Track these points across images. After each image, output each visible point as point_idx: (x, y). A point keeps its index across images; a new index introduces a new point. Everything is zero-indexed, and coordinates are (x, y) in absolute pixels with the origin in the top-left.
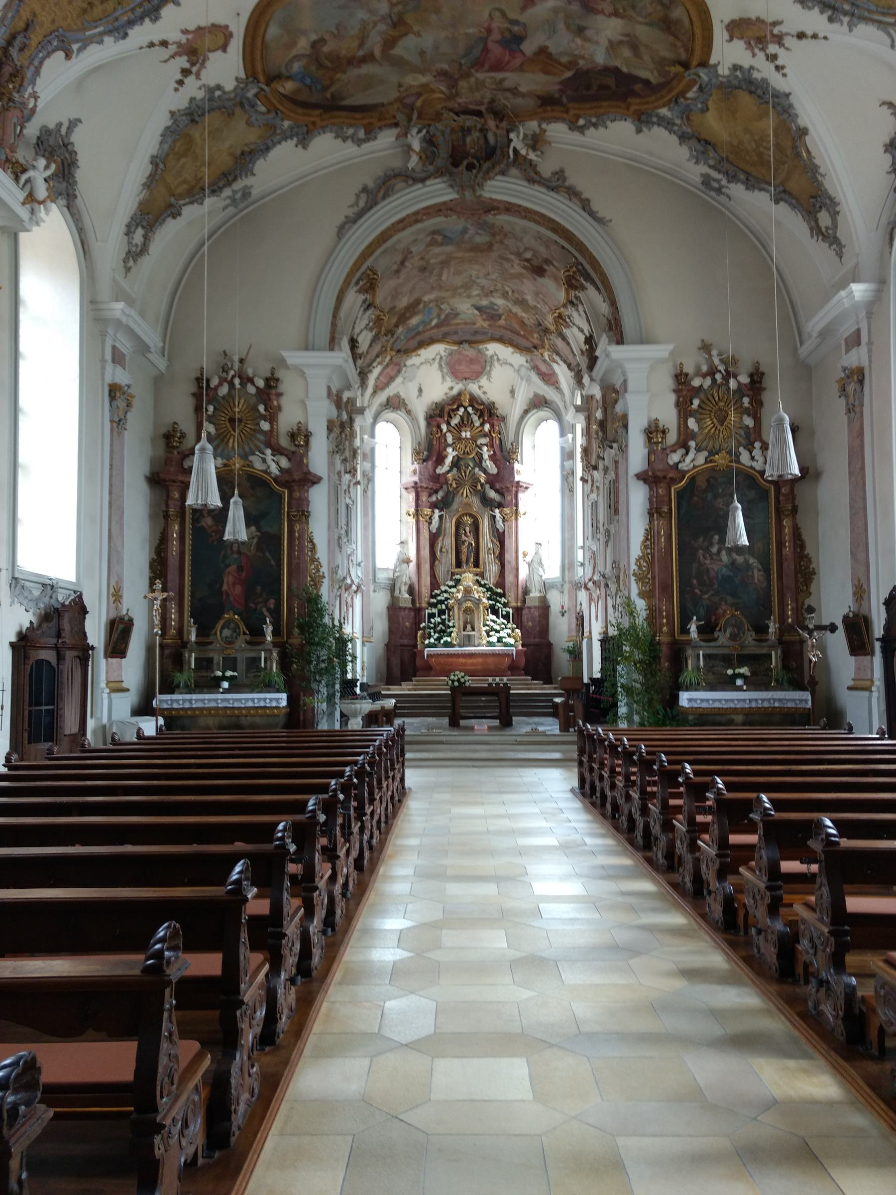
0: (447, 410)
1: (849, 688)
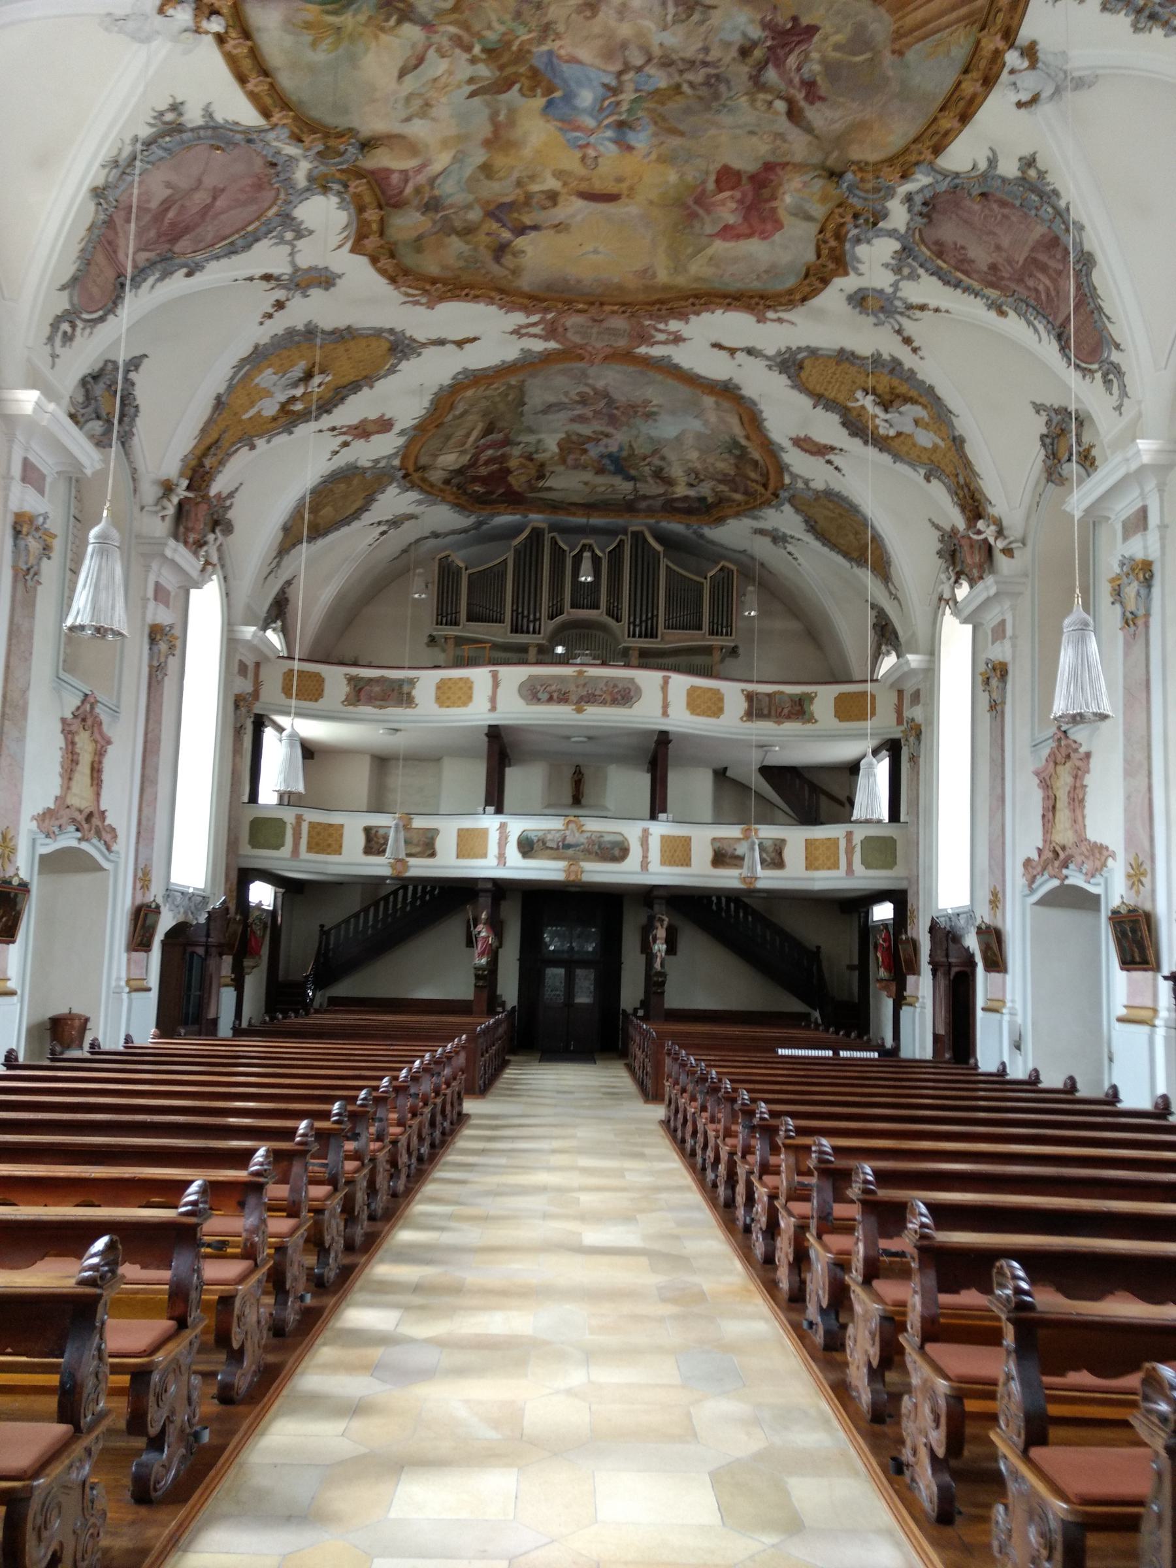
1: (1121, 1020)
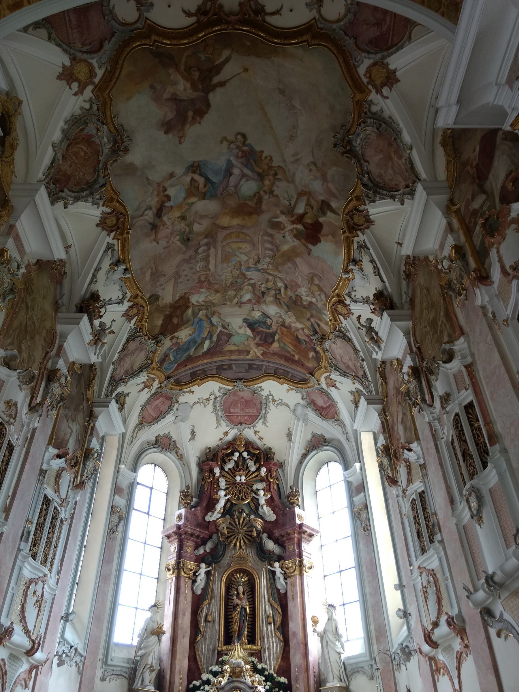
0: (220, 454)
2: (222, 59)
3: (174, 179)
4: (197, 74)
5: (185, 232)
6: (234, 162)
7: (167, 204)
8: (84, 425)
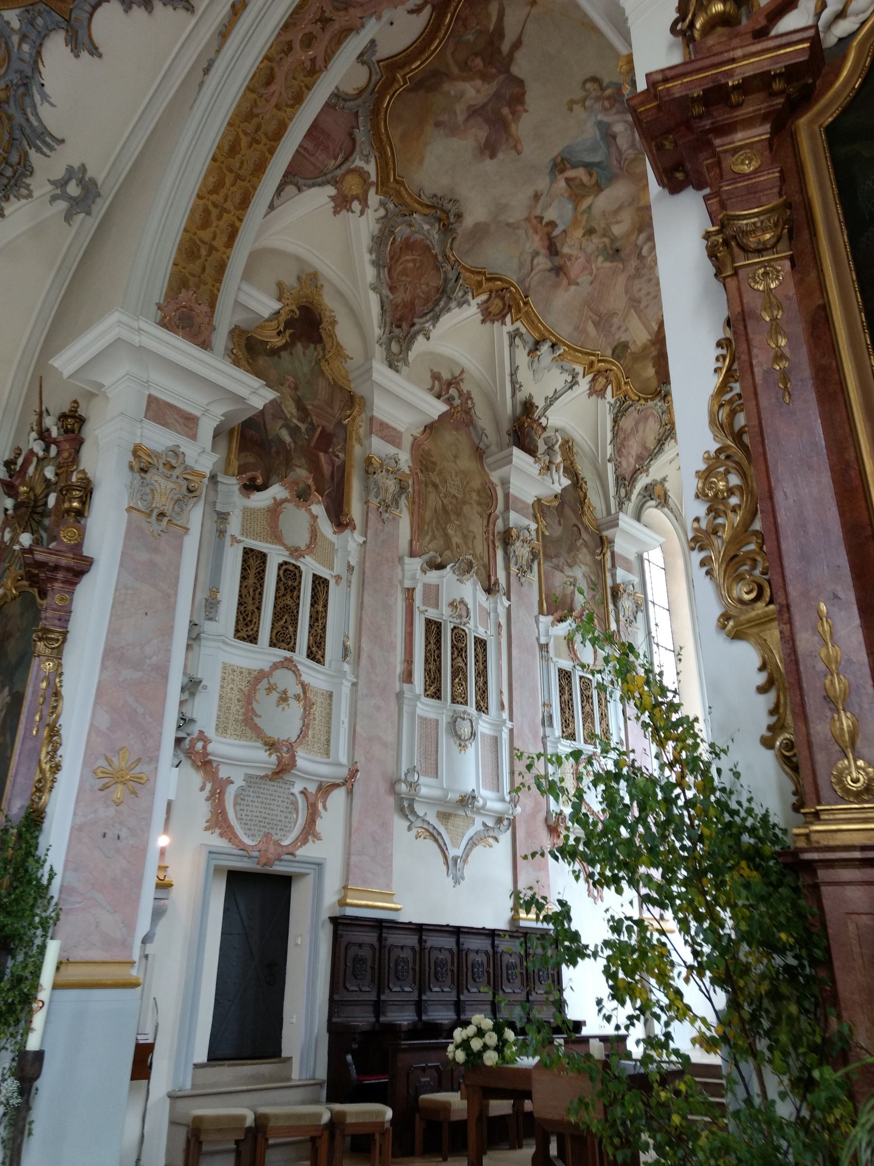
2: (494, 18)
3: (542, 200)
4: (478, 62)
5: (605, 245)
6: (606, 119)
7: (556, 233)
8: (595, 561)
